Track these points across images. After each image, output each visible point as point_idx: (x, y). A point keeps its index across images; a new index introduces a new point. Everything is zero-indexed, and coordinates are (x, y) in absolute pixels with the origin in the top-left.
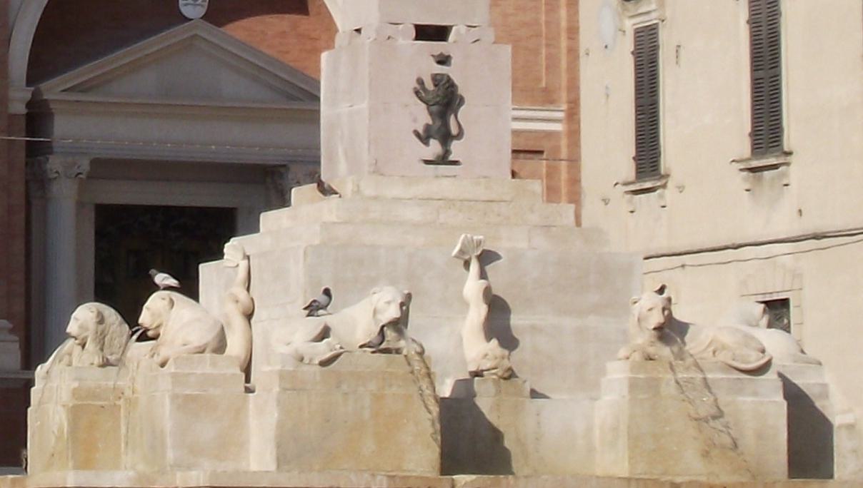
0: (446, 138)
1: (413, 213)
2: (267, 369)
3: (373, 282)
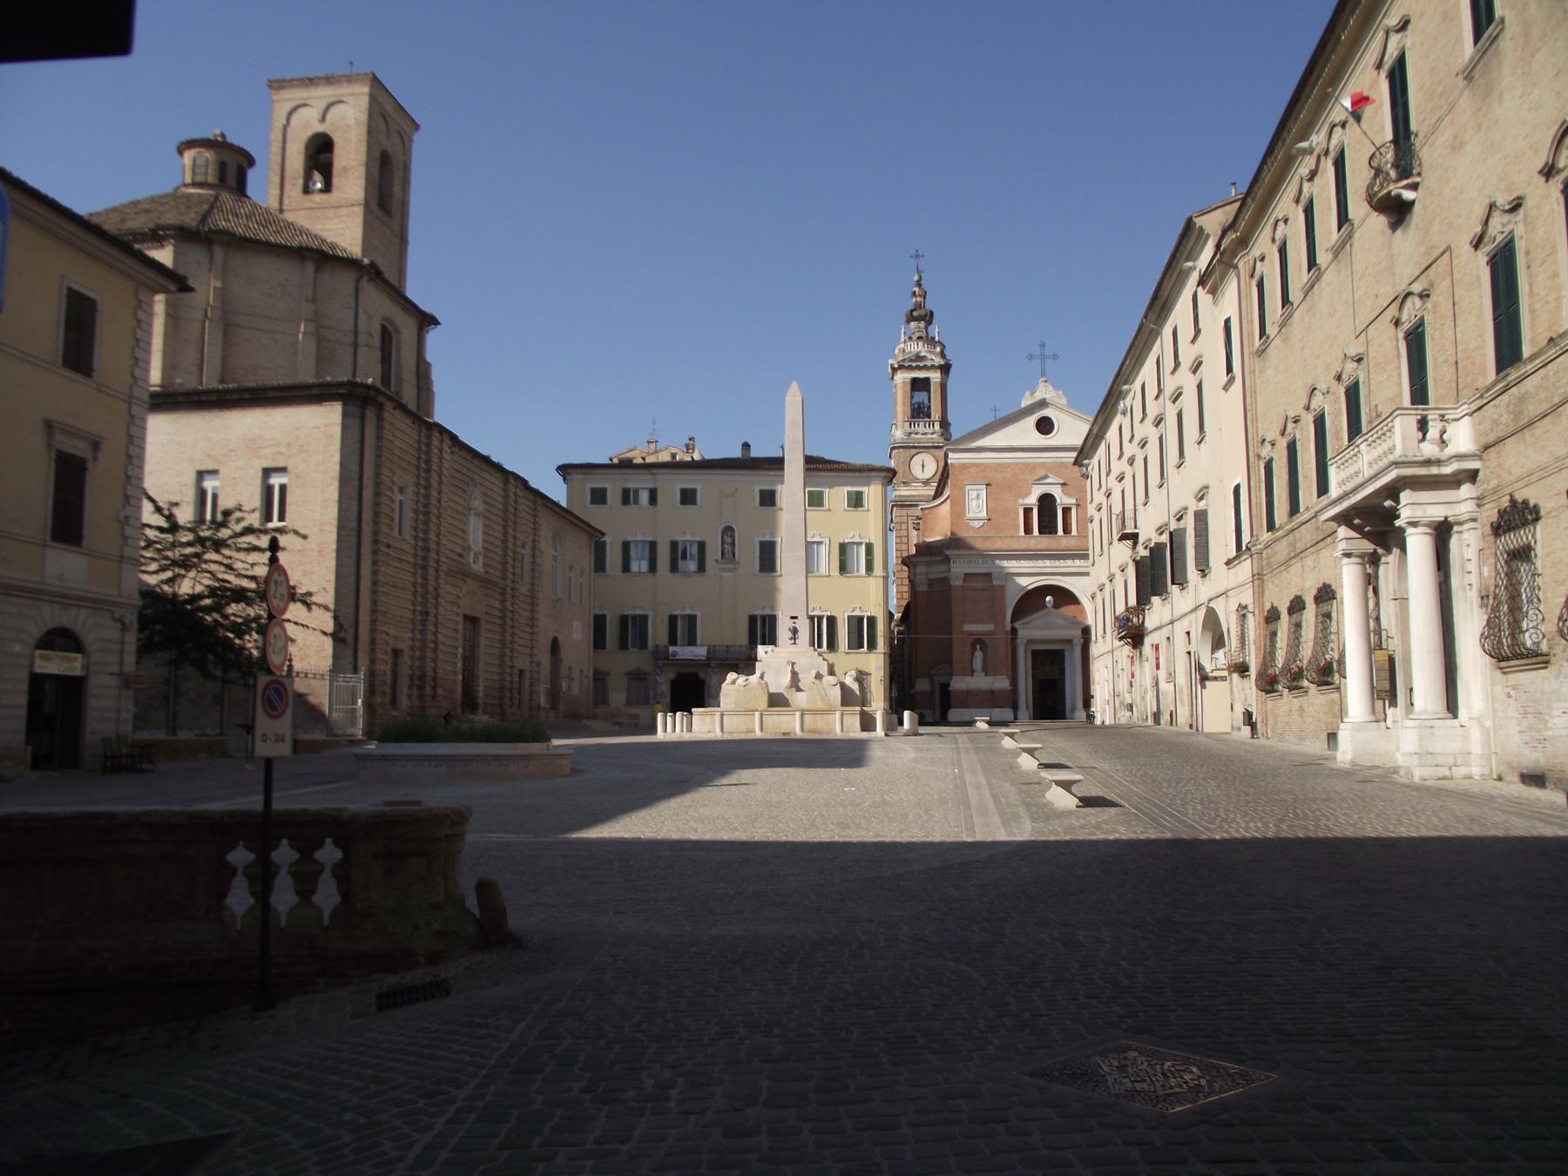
0: (795, 639)
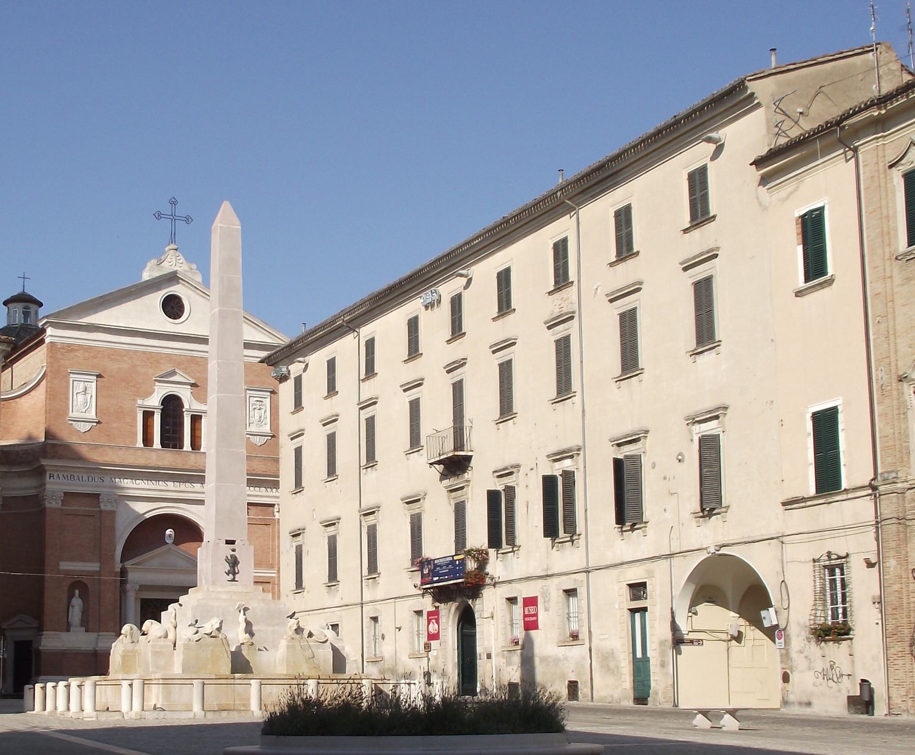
0: (234, 574)
1: (224, 596)
2: (180, 643)
3: (212, 617)
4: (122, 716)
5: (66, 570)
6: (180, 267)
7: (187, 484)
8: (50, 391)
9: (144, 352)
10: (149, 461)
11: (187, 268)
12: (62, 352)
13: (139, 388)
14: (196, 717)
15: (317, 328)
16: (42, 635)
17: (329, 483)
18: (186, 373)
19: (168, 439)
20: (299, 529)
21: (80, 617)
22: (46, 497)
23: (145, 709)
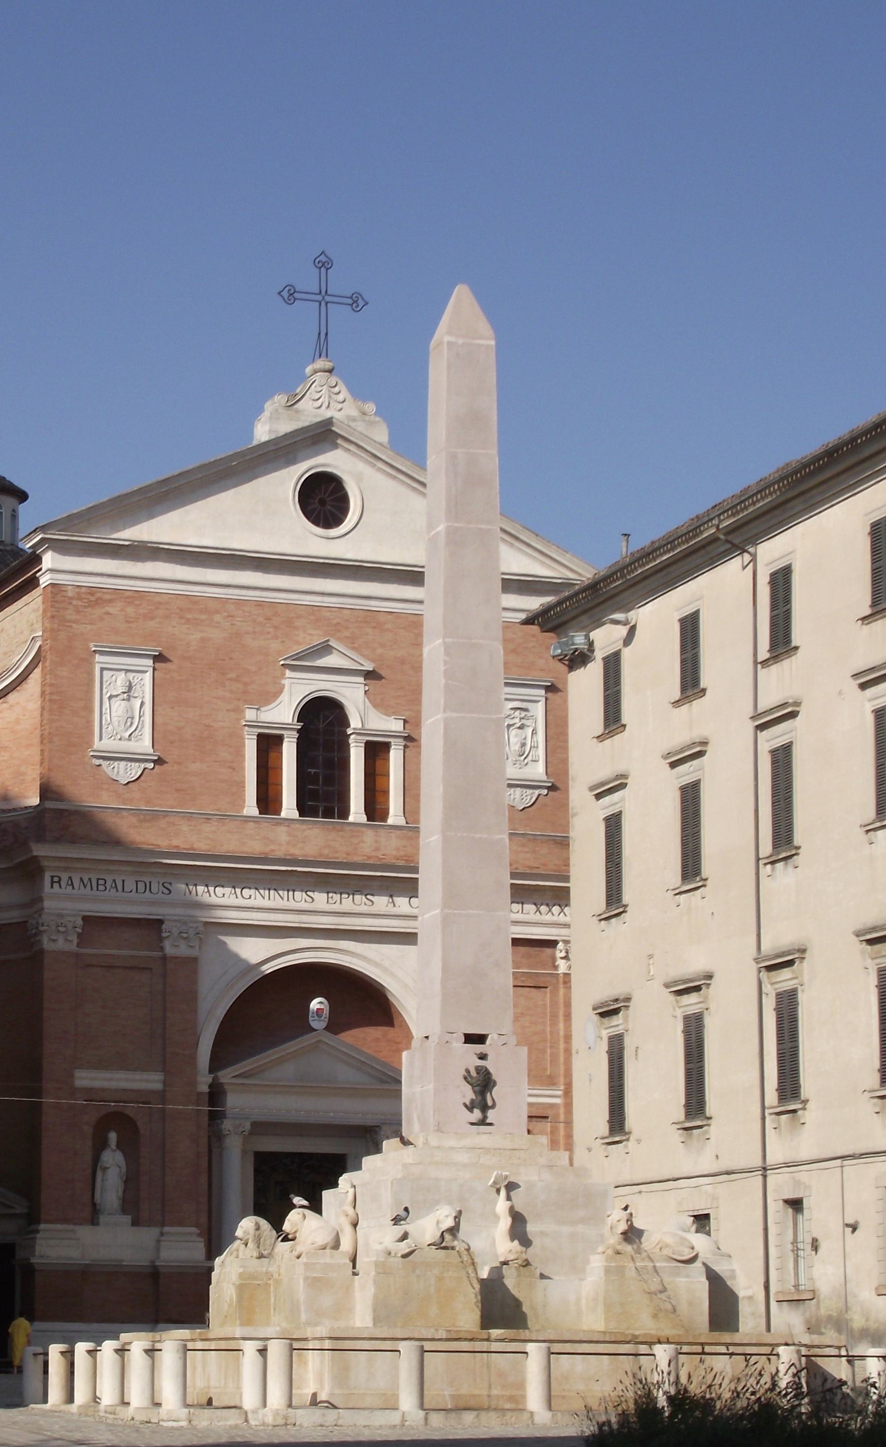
0: (484, 1108)
1: (463, 1158)
3: (437, 1202)
4: (244, 1417)
5: (89, 1090)
6: (340, 410)
7: (358, 897)
8: (51, 694)
9: (260, 604)
10: (272, 847)
11: (354, 413)
12: (75, 606)
13: (246, 684)
14: (407, 1423)
15: (656, 545)
16: (38, 1231)
17: (684, 895)
18: (353, 649)
19: (314, 795)
20: (616, 1000)
21: (120, 1193)
22: (45, 928)
23: (294, 1404)
